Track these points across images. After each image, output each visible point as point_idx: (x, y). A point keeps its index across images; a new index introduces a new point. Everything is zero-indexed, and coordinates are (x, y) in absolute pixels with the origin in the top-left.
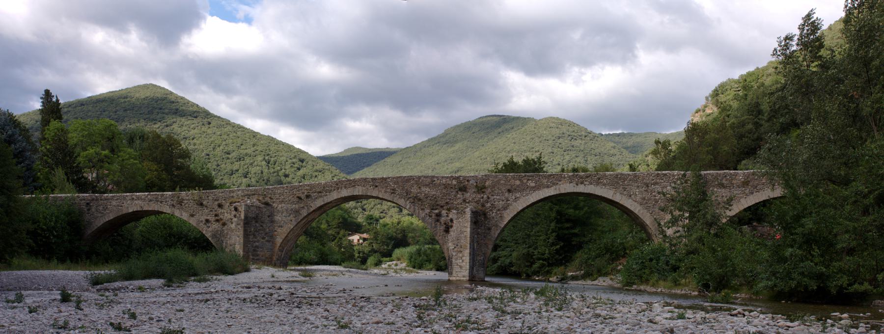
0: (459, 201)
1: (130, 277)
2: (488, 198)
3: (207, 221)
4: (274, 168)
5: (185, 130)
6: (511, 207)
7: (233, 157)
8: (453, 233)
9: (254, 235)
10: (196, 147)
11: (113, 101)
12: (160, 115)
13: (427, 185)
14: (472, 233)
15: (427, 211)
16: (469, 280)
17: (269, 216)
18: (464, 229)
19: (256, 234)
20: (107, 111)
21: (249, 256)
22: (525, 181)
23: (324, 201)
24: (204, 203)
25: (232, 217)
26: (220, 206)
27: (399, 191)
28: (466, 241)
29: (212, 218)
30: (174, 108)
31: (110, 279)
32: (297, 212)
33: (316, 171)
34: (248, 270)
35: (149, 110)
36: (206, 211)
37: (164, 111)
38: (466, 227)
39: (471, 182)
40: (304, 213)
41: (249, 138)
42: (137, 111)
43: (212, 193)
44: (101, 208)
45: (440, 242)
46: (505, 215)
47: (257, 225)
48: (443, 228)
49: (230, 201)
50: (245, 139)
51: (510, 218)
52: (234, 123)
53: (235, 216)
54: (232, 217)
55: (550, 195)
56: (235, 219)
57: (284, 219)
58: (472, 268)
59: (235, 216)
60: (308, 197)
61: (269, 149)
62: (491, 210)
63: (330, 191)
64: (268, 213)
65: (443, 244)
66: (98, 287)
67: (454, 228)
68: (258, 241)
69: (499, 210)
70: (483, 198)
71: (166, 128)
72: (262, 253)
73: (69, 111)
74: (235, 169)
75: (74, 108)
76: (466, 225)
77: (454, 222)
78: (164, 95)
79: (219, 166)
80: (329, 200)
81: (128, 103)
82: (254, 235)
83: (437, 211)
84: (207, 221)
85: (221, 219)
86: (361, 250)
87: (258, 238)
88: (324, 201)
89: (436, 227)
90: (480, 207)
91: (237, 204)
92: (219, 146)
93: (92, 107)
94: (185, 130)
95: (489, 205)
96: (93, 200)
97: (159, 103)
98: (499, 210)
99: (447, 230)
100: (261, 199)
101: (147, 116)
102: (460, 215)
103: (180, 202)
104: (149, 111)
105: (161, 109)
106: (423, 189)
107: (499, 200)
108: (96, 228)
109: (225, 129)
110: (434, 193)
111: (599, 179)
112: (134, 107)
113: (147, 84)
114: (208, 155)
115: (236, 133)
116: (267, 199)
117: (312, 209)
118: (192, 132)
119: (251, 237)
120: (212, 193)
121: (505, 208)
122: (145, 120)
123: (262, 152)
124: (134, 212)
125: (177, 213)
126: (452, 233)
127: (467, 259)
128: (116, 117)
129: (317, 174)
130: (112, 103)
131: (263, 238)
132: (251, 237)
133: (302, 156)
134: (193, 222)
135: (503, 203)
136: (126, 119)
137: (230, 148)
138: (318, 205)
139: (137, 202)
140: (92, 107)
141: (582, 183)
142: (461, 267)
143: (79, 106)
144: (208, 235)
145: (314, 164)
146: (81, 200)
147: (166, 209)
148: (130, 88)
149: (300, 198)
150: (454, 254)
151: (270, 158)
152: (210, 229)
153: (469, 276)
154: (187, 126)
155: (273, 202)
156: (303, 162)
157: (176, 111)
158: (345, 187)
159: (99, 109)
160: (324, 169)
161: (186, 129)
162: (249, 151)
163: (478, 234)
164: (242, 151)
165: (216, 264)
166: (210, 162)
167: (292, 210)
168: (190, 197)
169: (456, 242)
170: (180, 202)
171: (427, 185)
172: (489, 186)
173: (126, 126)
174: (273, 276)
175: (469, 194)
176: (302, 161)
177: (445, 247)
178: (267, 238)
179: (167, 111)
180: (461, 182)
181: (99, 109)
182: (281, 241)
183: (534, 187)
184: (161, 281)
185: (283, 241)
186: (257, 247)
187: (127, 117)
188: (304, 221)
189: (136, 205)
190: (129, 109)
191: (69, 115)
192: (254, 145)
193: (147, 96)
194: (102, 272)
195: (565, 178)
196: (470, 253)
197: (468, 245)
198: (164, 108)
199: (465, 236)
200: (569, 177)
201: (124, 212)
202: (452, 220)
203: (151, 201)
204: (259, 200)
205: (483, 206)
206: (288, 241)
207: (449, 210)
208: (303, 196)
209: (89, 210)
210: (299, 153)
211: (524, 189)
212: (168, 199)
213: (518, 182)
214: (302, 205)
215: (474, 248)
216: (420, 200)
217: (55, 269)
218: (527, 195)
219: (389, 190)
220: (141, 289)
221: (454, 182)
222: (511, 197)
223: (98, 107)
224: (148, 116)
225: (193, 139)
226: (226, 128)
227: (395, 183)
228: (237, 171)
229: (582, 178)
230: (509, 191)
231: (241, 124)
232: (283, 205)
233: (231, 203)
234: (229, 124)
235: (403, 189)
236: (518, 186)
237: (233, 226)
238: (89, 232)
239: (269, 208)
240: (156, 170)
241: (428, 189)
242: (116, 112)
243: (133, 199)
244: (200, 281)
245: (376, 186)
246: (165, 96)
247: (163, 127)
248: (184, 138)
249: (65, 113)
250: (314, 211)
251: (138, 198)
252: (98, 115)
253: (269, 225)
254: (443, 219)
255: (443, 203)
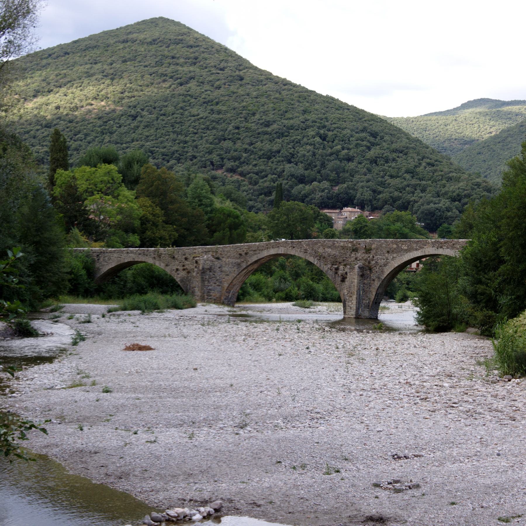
0: (353, 259)
1: (125, 309)
2: (373, 257)
3: (177, 270)
4: (331, 148)
5: (206, 91)
6: (389, 264)
7: (273, 130)
8: (347, 283)
9: (209, 281)
10: (221, 116)
11: (108, 47)
12: (172, 67)
13: (329, 247)
14: (359, 283)
15: (329, 266)
16: (355, 318)
17: (219, 268)
18: (353, 280)
19: (210, 280)
20: (100, 62)
21: (204, 296)
22: (400, 245)
23: (257, 257)
24: (176, 257)
25: (194, 267)
26: (186, 259)
27: (309, 251)
28: (355, 290)
29: (181, 268)
30: (192, 55)
31: (116, 310)
32: (239, 265)
33: (395, 151)
34: (193, 306)
35: (157, 60)
36: (177, 262)
37: (178, 62)
38: (355, 279)
39: (361, 245)
40: (244, 265)
41: (299, 101)
42: (140, 62)
43: (181, 249)
44: (106, 258)
45: (338, 289)
46: (385, 270)
47: (211, 273)
48: (340, 279)
49: (193, 256)
50: (292, 102)
51: (388, 272)
52: (277, 77)
53: (196, 267)
54: (194, 267)
55: (418, 256)
56: (196, 269)
57: (230, 270)
58: (357, 309)
59: (196, 267)
60: (246, 254)
61: (326, 118)
62: (375, 266)
63: (262, 250)
64: (219, 265)
65: (340, 291)
66: (111, 313)
67: (348, 279)
68: (211, 286)
69: (381, 266)
70: (369, 257)
71: (180, 88)
72: (214, 294)
73: (49, 64)
74: (275, 148)
75: (55, 59)
76: (354, 277)
77: (348, 274)
78: (178, 35)
79: (252, 144)
80: (261, 257)
81: (128, 49)
82: (209, 281)
83: (336, 266)
84: (177, 270)
85: (187, 269)
86: (410, 280)
87: (211, 283)
88: (257, 257)
89: (335, 278)
90: (367, 264)
91: (197, 258)
92: (254, 114)
93: (80, 57)
94: (206, 91)
95: (373, 262)
96: (101, 252)
97: (172, 49)
98: (381, 266)
99: (343, 279)
100: (214, 254)
101: (155, 68)
102: (351, 270)
103: (159, 256)
104: (157, 62)
105: (173, 58)
106: (327, 250)
107: (381, 259)
108: (103, 273)
109: (264, 87)
110: (334, 253)
111: (454, 244)
112: (136, 56)
113: (156, 18)
114: (238, 128)
115: (280, 94)
116: (218, 255)
117: (249, 263)
118: (217, 93)
119: (206, 282)
120: (181, 249)
121: (385, 265)
122: (151, 75)
123: (316, 122)
124: (128, 262)
125: (157, 264)
126: (346, 283)
127: (354, 302)
128: (111, 71)
129: (394, 155)
130: (107, 50)
131: (215, 283)
132: (206, 282)
133: (375, 128)
134: (168, 270)
135: (384, 261)
136: (125, 74)
137: (271, 117)
138: (254, 260)
139: (130, 255)
140: (80, 57)
141: (441, 247)
142: (351, 308)
143: (62, 56)
144: (178, 280)
145: (393, 139)
146: (93, 253)
147: (150, 261)
148: (132, 25)
149: (241, 255)
150: (347, 298)
151: (327, 132)
152: (179, 276)
153: (356, 315)
154: (210, 84)
155: (223, 257)
156: (376, 138)
157: (194, 61)
158: (273, 247)
159: (89, 60)
160: (407, 148)
161: (208, 88)
162: (295, 122)
163: (364, 284)
164: (287, 121)
165: (172, 303)
166: (240, 139)
167: (235, 263)
168: (166, 252)
169: (348, 289)
170: (159, 256)
171: (329, 247)
172: (374, 248)
173: (125, 86)
174: (206, 311)
175: (360, 254)
176: (374, 135)
177: (342, 293)
178: (217, 284)
179: (182, 60)
180: (354, 245)
181: (89, 60)
182: (227, 285)
183: (406, 250)
184: (140, 312)
185: (229, 285)
186: (210, 290)
187: (125, 71)
188: (244, 271)
189: (130, 257)
190: (130, 58)
191: (48, 70)
192: (305, 112)
193: (154, 38)
194: (113, 305)
195: (429, 243)
196: (357, 298)
197: (356, 292)
198: (178, 55)
199: (354, 286)
200: (432, 242)
201: (122, 262)
202: (346, 273)
203: (140, 254)
204: (213, 256)
205: (369, 263)
206: (234, 285)
207: (345, 265)
208: (243, 254)
209: (98, 260)
210: (371, 123)
211: (399, 251)
212: (151, 254)
213: (395, 246)
214: (243, 260)
215: (360, 295)
216: (324, 257)
217: (80, 303)
218: (401, 255)
219: (302, 250)
220: (129, 315)
221: (350, 245)
222: (390, 257)
223: (88, 58)
224: (155, 69)
225: (217, 103)
226: (265, 85)
227: (307, 245)
228: (279, 152)
229: (441, 243)
230: (388, 252)
231: (288, 79)
232: (230, 259)
233: (194, 257)
234: (270, 79)
235: (312, 250)
236: (395, 249)
237: (194, 274)
238: (98, 275)
239: (220, 261)
240: (151, 206)
241: (330, 250)
242: (111, 64)
243: (128, 253)
244: (159, 312)
245: (294, 247)
246: (180, 37)
247: (175, 86)
248: (204, 103)
249: (44, 67)
250: (251, 264)
251: (132, 252)
252: (88, 69)
253: (219, 273)
254: (340, 272)
255: (341, 260)
